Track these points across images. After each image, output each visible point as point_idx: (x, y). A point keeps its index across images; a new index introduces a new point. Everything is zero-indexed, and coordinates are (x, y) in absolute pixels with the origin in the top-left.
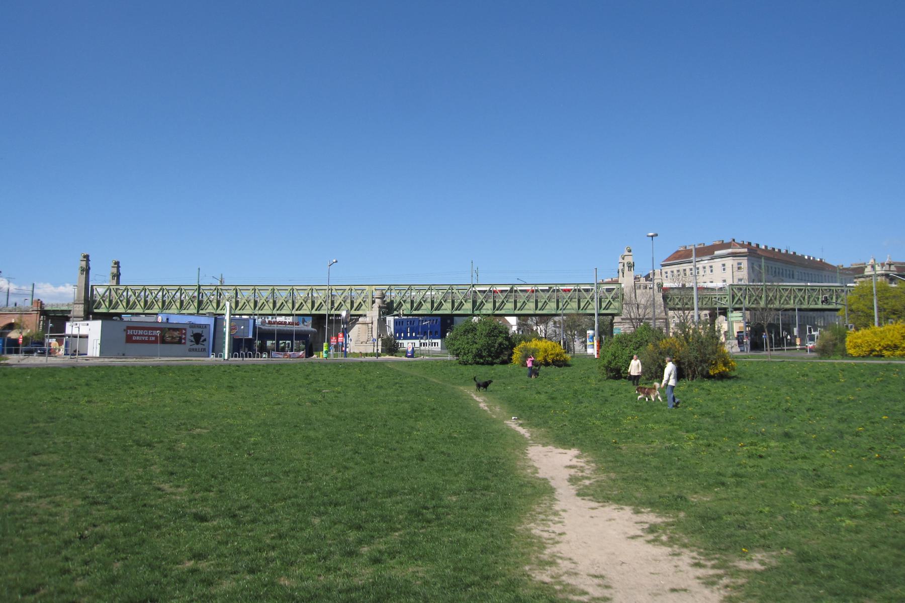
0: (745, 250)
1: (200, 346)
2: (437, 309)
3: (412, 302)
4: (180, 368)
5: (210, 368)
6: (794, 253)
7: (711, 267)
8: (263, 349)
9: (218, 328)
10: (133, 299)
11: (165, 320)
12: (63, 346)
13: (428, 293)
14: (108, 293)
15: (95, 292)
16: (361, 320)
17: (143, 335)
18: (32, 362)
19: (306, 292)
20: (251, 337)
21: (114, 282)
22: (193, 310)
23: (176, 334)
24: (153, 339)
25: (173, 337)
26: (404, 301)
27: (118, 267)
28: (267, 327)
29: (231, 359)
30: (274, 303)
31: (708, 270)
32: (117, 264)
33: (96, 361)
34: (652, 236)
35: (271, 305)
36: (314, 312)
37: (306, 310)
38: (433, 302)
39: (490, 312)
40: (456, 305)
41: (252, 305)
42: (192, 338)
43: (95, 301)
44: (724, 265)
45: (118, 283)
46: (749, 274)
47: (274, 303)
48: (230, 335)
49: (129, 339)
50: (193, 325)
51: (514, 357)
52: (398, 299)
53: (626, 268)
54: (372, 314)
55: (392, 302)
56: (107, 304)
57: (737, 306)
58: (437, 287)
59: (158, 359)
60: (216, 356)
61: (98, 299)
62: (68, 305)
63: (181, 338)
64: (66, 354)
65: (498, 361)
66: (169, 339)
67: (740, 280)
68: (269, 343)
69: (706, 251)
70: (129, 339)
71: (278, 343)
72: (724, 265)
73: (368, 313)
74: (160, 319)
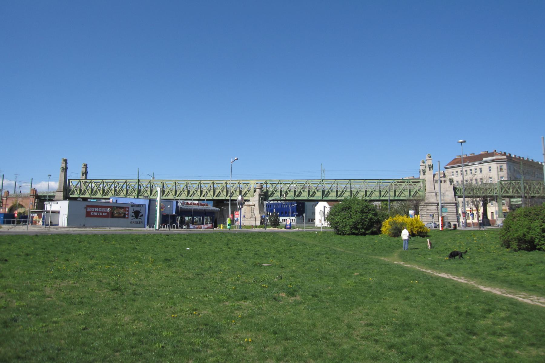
0: (505, 157)
1: (138, 220)
2: (298, 196)
3: (295, 192)
4: (122, 237)
5: (146, 236)
6: (533, 160)
7: (481, 169)
8: (182, 222)
9: (151, 207)
10: (106, 188)
11: (115, 201)
12: (42, 219)
13: (292, 186)
14: (79, 185)
15: (71, 184)
16: (246, 203)
17: (98, 212)
18: (18, 230)
19: (209, 185)
20: (174, 213)
21: (84, 178)
22: (134, 195)
23: (122, 211)
24: (106, 214)
25: (119, 214)
26: (276, 191)
27: (86, 168)
28: (185, 207)
29: (160, 229)
30: (189, 192)
31: (478, 171)
32: (86, 165)
33: (63, 230)
34: (462, 143)
35: (186, 193)
36: (215, 198)
37: (210, 196)
38: (295, 192)
39: (334, 198)
40: (311, 193)
41: (174, 193)
42: (133, 214)
43: (70, 190)
44: (490, 167)
45: (86, 178)
46: (508, 174)
47: (189, 192)
48: (160, 212)
49: (88, 214)
50: (133, 205)
51: (383, 229)
52: (271, 189)
53: (428, 168)
54: (254, 199)
55: (267, 191)
56: (78, 192)
57: (504, 195)
58: (284, 182)
59: (108, 229)
60: (150, 227)
61: (73, 188)
62: (54, 192)
63: (125, 214)
64: (43, 225)
65: (369, 232)
66: (117, 214)
67: (502, 177)
68: (187, 218)
69: (478, 158)
70: (88, 214)
71: (193, 219)
72: (490, 167)
73: (251, 199)
74: (111, 201)
